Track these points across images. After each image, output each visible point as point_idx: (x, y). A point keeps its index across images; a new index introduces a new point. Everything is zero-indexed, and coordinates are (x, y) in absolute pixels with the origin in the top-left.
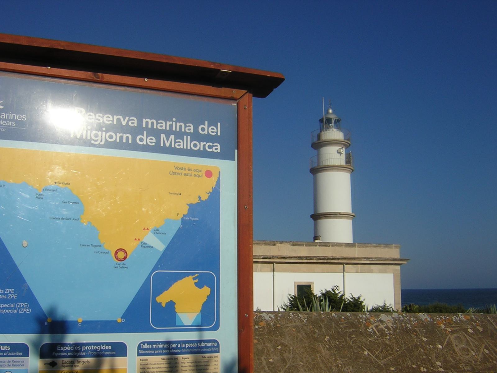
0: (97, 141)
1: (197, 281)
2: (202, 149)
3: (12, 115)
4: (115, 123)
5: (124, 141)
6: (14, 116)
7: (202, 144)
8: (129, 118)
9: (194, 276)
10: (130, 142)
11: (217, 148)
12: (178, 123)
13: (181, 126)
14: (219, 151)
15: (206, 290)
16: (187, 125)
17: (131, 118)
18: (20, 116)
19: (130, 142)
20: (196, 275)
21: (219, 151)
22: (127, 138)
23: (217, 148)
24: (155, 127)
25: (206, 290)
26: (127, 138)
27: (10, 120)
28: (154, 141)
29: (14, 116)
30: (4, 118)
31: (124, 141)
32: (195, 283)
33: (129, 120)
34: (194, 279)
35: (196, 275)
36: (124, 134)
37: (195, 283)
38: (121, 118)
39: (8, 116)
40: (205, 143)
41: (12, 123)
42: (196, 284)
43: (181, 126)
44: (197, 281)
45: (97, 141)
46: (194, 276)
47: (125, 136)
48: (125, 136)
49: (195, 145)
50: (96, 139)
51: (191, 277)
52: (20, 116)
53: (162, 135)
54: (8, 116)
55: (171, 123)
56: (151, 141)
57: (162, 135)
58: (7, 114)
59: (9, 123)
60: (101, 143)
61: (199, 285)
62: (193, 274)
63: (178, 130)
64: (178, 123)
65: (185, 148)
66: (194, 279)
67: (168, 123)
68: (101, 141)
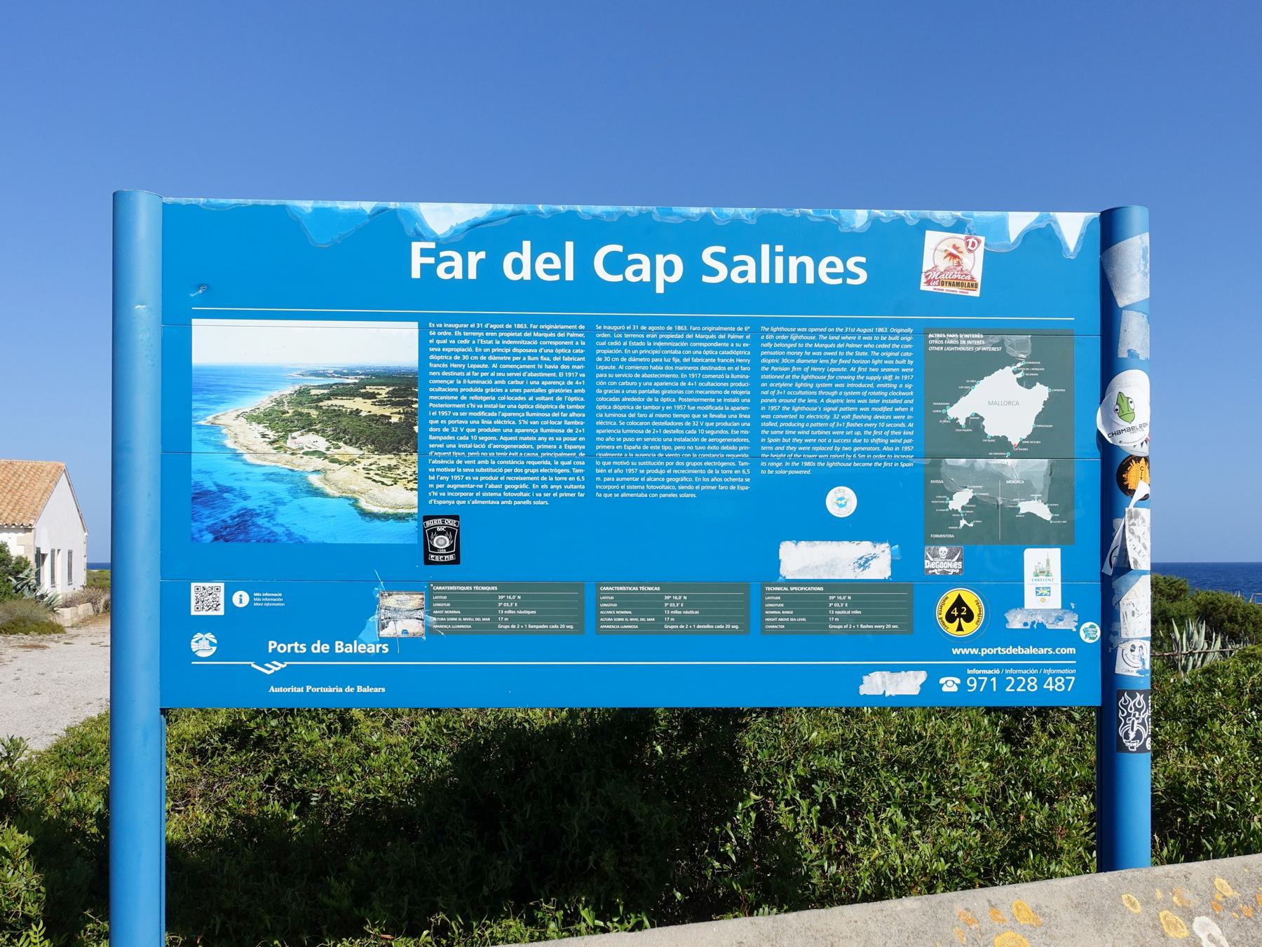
15: (1041, 393)
25: (1041, 393)
32: (1018, 380)
37: (1018, 380)
42: (1020, 381)
44: (1020, 375)
51: (1009, 369)
61: (1026, 382)
66: (1015, 372)
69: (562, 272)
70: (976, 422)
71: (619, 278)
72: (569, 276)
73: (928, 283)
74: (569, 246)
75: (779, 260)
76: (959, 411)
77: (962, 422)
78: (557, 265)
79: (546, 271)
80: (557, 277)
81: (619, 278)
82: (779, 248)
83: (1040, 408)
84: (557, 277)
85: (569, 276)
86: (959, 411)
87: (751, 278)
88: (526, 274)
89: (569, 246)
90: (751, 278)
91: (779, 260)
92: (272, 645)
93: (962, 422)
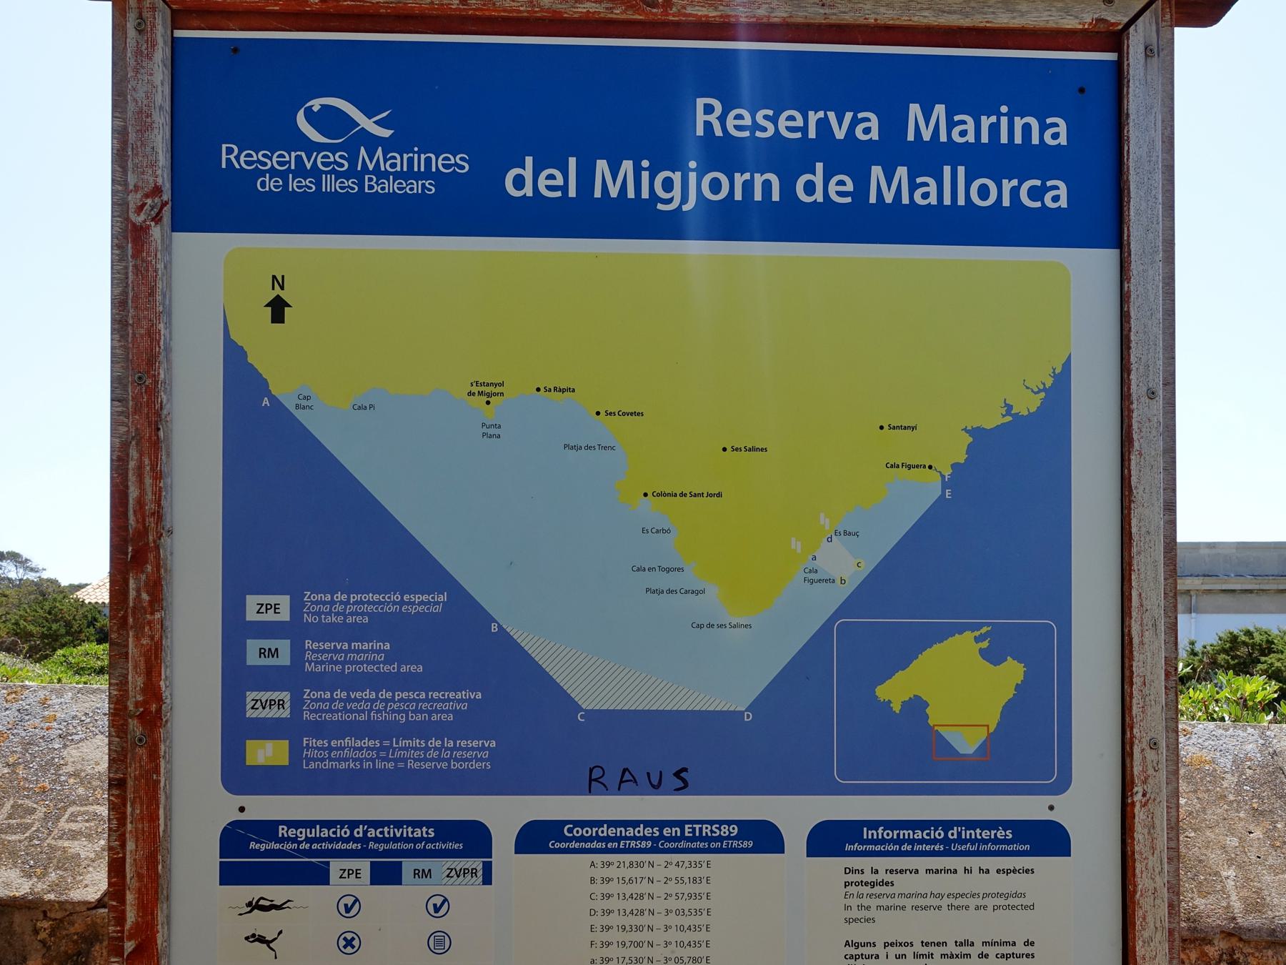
0: (670, 201)
1: (985, 644)
2: (1006, 202)
3: (423, 157)
4: (812, 134)
5: (758, 196)
6: (428, 160)
7: (1007, 185)
8: (855, 117)
9: (977, 633)
10: (776, 197)
11: (1059, 195)
12: (1017, 119)
13: (1027, 129)
14: (1065, 205)
15: (1013, 672)
16: (1049, 121)
17: (860, 115)
18: (250, 156)
19: (776, 197)
20: (984, 630)
21: (1065, 205)
22: (767, 185)
23: (1059, 195)
24: (1035, 140)
25: (1013, 672)
26: (767, 185)
27: (418, 176)
28: (850, 187)
29: (428, 160)
30: (398, 169)
31: (758, 196)
32: (981, 651)
33: (855, 122)
34: (977, 640)
35: (984, 630)
36: (757, 176)
37: (981, 651)
38: (832, 116)
39: (411, 160)
40: (1015, 182)
41: (423, 185)
42: (982, 652)
43: (1027, 129)
44: (985, 644)
45: (670, 201)
46: (977, 633)
47: (759, 179)
48: (759, 179)
49: (984, 193)
50: (667, 196)
51: (969, 636)
52: (250, 156)
53: (873, 168)
54: (411, 160)
55: (993, 119)
56: (840, 188)
57: (873, 168)
58: (405, 156)
59: (416, 187)
60: (685, 208)
61: (993, 656)
62: (974, 627)
63: (1018, 140)
64: (1017, 119)
65: (947, 201)
66: (977, 640)
67: (986, 122)
68: (684, 199)
69: (564, 189)
70: (916, 707)
71: (1038, 204)
72: (572, 193)
73: (357, 872)
74: (572, 162)
75: (645, 175)
76: (894, 691)
77: (897, 708)
78: (559, 181)
79: (548, 187)
80: (559, 194)
81: (1038, 204)
82: (645, 163)
83: (1010, 693)
84: (559, 194)
85: (572, 193)
86: (894, 691)
87: (933, 200)
88: (528, 191)
89: (572, 162)
90: (933, 200)
91: (645, 175)
92: (451, 718)
93: (897, 708)
